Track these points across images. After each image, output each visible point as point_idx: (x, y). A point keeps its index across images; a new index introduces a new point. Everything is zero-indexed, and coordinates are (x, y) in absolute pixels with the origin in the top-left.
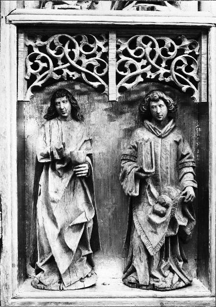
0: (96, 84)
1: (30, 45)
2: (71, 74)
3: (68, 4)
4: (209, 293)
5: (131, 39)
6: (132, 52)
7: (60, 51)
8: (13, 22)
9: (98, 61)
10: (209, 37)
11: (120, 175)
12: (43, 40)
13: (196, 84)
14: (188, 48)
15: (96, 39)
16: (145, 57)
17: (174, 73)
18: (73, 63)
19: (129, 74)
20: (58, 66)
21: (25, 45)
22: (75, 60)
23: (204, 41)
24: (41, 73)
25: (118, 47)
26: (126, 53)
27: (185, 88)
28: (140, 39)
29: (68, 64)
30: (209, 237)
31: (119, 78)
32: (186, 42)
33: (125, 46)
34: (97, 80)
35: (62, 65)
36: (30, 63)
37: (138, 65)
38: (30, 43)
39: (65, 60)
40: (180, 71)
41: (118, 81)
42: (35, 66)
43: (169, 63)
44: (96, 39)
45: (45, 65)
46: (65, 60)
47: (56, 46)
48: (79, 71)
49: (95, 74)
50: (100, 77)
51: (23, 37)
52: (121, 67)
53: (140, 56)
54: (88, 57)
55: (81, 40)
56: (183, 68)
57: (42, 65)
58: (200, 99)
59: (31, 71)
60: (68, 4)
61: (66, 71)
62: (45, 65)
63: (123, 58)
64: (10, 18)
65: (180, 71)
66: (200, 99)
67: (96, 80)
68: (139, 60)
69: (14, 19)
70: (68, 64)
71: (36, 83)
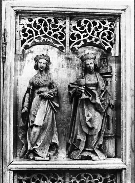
0: (58, 46)
1: (21, 179)
2: (45, 39)
3: (42, 158)
4: (121, 162)
5: (77, 175)
6: (78, 28)
7: (39, 27)
8: (11, 170)
9: (60, 33)
10: (121, 19)
11: (71, 116)
12: (28, 176)
13: (112, 45)
14: (110, 179)
15: (58, 175)
16: (85, 31)
17: (101, 40)
18: (46, 33)
19: (77, 40)
20: (38, 35)
21: (18, 179)
22: (47, 32)
23: (118, 23)
24: (28, 39)
25: (71, 24)
26: (75, 28)
27: (106, 48)
28: (82, 175)
29: (44, 35)
30: (121, 128)
31: (71, 43)
32: (108, 23)
33: (75, 23)
34: (59, 44)
35: (40, 34)
36: (22, 34)
37: (82, 35)
38: (21, 178)
39: (42, 32)
40: (104, 39)
41: (70, 44)
42: (25, 35)
43: (98, 34)
44: (58, 175)
45: (31, 35)
46: (42, 32)
47: (35, 180)
48: (49, 38)
49: (58, 40)
50: (61, 42)
51: (16, 175)
52: (72, 36)
53: (83, 31)
54: (54, 31)
55: (50, 176)
56: (106, 37)
57: (29, 35)
58: (115, 54)
59: (23, 37)
60: (42, 158)
61: (43, 38)
62: (31, 35)
63: (74, 31)
64: (10, 167)
65: (104, 39)
66: (115, 54)
67: (58, 43)
68: (82, 32)
69: (12, 168)
70: (44, 35)
71: (26, 43)
